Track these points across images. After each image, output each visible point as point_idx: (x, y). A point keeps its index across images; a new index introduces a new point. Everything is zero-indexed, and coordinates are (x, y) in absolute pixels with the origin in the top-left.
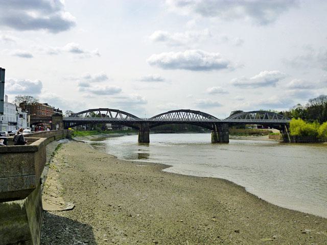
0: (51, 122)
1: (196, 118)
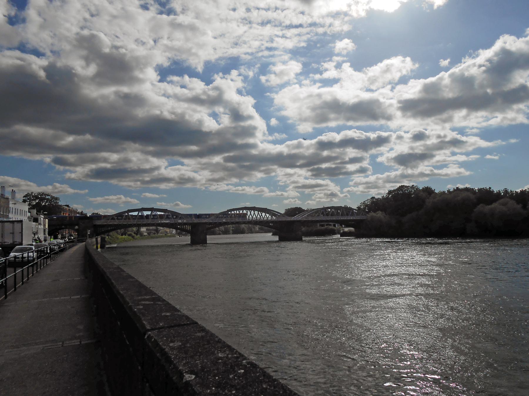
0: (77, 227)
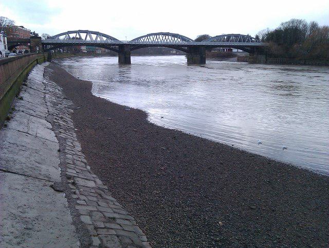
0: (29, 44)
1: (157, 40)
